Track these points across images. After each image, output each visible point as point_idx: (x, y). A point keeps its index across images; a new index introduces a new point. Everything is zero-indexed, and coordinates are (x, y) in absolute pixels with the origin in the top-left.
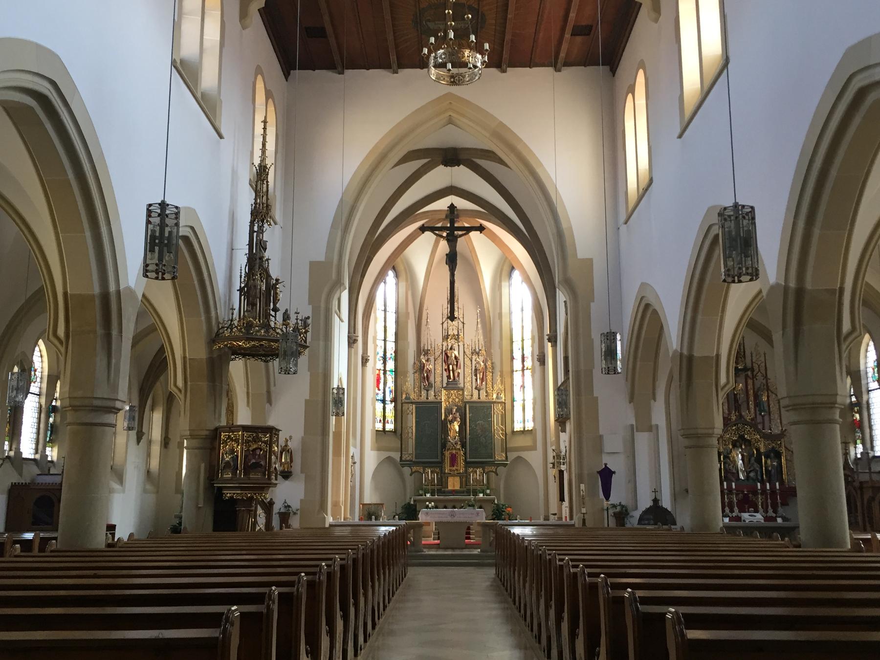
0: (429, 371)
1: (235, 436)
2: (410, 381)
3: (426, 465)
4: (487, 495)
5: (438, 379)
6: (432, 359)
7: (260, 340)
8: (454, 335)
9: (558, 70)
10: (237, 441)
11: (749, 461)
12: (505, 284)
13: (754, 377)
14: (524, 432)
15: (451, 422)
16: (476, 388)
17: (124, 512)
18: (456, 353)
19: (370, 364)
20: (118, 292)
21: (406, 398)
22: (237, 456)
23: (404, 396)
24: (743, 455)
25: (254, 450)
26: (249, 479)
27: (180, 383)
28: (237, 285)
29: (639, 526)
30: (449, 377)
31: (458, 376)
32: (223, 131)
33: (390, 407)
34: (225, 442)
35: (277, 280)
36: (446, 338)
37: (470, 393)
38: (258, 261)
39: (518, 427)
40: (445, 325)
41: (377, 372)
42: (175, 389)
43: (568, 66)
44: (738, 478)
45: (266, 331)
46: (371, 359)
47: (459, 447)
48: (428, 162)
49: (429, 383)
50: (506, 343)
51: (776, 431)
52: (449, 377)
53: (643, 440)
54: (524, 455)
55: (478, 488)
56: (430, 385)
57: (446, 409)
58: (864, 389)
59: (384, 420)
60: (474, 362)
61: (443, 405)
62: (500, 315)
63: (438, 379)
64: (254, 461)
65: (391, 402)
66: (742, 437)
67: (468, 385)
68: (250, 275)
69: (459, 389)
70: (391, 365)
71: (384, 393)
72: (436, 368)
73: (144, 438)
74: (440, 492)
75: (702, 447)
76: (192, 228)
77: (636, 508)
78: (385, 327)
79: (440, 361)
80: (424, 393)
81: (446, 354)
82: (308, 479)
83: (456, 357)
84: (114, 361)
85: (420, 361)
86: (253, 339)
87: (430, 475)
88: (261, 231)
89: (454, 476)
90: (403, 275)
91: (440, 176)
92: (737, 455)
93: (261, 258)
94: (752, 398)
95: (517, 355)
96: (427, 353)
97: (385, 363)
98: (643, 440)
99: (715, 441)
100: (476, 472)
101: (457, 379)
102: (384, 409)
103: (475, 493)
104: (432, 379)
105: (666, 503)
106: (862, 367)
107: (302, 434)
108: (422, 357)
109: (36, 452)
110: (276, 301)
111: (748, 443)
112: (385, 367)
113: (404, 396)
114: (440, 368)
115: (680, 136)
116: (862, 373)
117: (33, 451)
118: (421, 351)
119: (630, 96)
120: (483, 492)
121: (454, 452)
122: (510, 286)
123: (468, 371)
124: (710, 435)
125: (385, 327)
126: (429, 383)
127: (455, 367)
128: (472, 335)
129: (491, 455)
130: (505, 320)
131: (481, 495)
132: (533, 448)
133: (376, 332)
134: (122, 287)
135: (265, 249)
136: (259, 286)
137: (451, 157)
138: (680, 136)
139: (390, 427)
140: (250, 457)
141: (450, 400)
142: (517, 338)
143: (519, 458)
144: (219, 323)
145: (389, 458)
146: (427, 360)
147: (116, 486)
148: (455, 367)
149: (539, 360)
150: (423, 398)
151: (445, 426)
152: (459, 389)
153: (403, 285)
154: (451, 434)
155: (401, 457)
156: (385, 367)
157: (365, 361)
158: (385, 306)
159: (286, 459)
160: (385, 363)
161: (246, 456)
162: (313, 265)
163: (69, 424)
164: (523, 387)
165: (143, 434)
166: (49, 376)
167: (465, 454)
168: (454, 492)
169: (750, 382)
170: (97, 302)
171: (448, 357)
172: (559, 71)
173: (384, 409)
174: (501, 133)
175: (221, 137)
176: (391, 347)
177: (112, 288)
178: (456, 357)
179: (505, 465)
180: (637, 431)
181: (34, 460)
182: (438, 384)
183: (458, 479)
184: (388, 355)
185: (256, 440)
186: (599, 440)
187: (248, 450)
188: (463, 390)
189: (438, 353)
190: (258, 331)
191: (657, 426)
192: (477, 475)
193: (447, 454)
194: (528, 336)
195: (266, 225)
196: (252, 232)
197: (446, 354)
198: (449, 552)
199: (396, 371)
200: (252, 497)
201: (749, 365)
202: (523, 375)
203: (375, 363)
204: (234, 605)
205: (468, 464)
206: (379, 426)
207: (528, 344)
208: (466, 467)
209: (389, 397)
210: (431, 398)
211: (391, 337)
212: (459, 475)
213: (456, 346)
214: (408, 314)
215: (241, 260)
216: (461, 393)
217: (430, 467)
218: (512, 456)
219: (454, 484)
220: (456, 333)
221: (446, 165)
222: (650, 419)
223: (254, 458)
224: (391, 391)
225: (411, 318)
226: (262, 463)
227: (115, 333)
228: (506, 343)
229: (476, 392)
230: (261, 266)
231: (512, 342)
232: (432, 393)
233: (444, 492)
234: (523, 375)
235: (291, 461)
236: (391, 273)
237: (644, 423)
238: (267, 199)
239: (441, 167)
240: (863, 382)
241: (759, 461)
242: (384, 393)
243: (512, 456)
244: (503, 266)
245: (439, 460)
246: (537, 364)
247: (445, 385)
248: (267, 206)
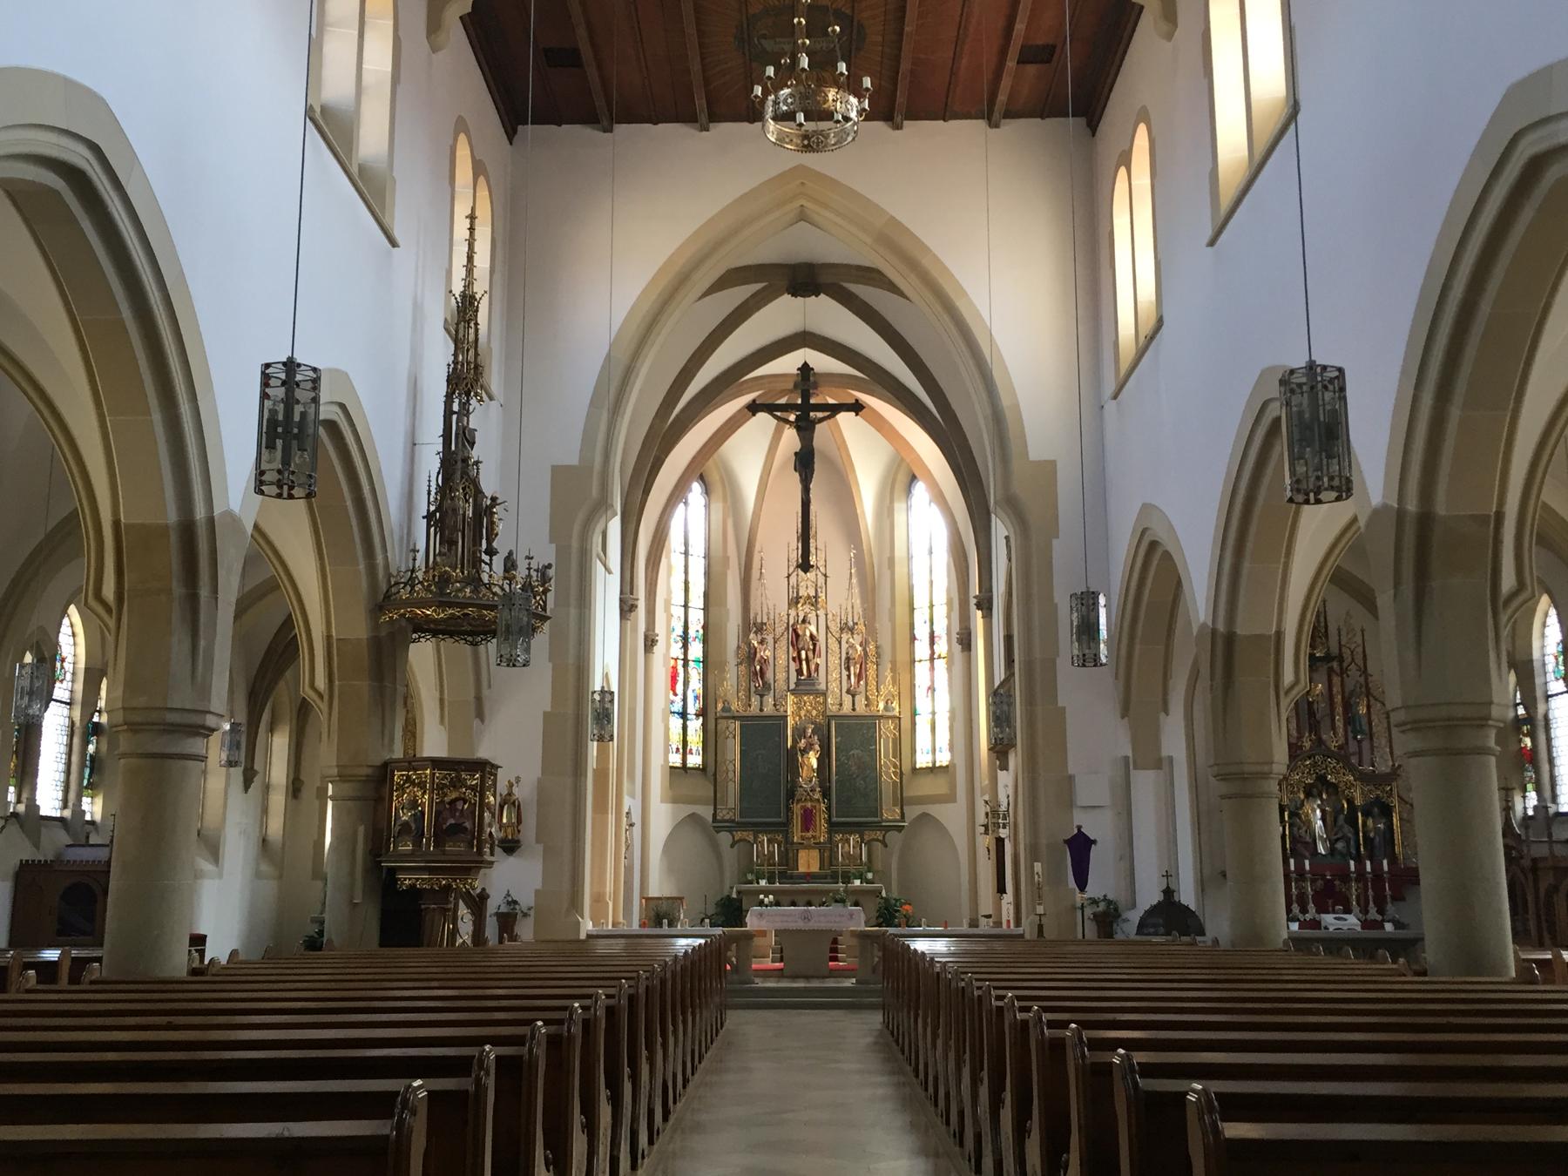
0: (764, 661)
1: (419, 776)
2: (731, 678)
3: (759, 828)
4: (868, 882)
5: (781, 676)
6: (770, 639)
7: (463, 606)
8: (809, 597)
9: (994, 124)
10: (422, 785)
11: (1335, 821)
12: (899, 506)
13: (1343, 672)
14: (933, 770)
15: (804, 751)
16: (848, 692)
17: (221, 912)
18: (813, 628)
19: (659, 649)
21: (723, 709)
22: (423, 813)
23: (720, 706)
24: (1323, 811)
25: (453, 802)
26: (444, 853)
27: (321, 682)
28: (422, 508)
29: (1138, 938)
30: (800, 672)
31: (817, 669)
32: (398, 234)
33: (695, 725)
34: (401, 788)
35: (494, 499)
36: (794, 602)
37: (838, 701)
38: (459, 464)
39: (923, 761)
40: (793, 579)
41: (672, 662)
42: (312, 693)
43: (1013, 117)
44: (1315, 852)
45: (474, 590)
46: (661, 639)
47: (817, 796)
48: (763, 289)
49: (765, 683)
50: (901, 610)
51: (1383, 767)
52: (800, 672)
53: (1145, 784)
54: (934, 810)
55: (852, 869)
56: (767, 687)
57: (795, 729)
58: (1539, 694)
59: (685, 749)
60: (844, 646)
61: (790, 722)
62: (892, 561)
63: (781, 676)
64: (452, 821)
65: (697, 715)
66: (1322, 779)
67: (834, 686)
68: (445, 490)
69: (818, 693)
70: (696, 650)
71: (685, 700)
72: (777, 656)
73: (257, 781)
74: (784, 877)
75: (1251, 796)
76: (342, 406)
77: (1134, 906)
78: (686, 583)
79: (783, 643)
80: (755, 700)
81: (795, 631)
82: (549, 853)
83: (812, 636)
84: (202, 643)
85: (749, 644)
86: (451, 605)
87: (765, 845)
88: (465, 411)
89: (808, 847)
90: (717, 490)
91: (784, 314)
92: (1314, 811)
93: (465, 460)
94: (1339, 709)
95: (922, 632)
96: (760, 628)
97: (685, 646)
98: (1145, 784)
99: (1274, 787)
100: (848, 841)
101: (814, 675)
102: (685, 728)
103: (847, 879)
104: (769, 675)
105: (1187, 896)
106: (1536, 655)
107: (539, 773)
108: (752, 636)
109: (65, 806)
110: (491, 536)
111: (1333, 789)
112: (686, 654)
113: (720, 706)
114: (784, 657)
115: (1212, 243)
116: (1537, 665)
117: (58, 804)
118: (751, 626)
119: (1122, 171)
120: (861, 876)
121: (809, 805)
122: (908, 509)
123: (834, 661)
124: (1265, 776)
125: (686, 583)
126: (765, 683)
127: (810, 654)
128: (841, 597)
129: (876, 812)
130: (900, 570)
131: (857, 882)
132: (950, 798)
133: (669, 592)
135: (472, 444)
136: (461, 510)
137: (804, 279)
138: (1212, 243)
139: (695, 760)
140: (446, 814)
141: (803, 713)
142: (921, 602)
143: (925, 815)
144: (390, 575)
145: (693, 816)
146: (762, 642)
147: (206, 866)
148: (810, 654)
149: (960, 641)
150: (754, 709)
151: (792, 760)
152: (818, 693)
153: (717, 507)
154: (804, 773)
155: (715, 815)
156: (686, 654)
157: (650, 643)
158: (686, 544)
159: (509, 817)
160: (685, 646)
161: (438, 813)
162: (557, 471)
164: (932, 689)
165: (255, 773)
166: (87, 670)
167: (829, 808)
168: (809, 877)
169: (1336, 680)
171: (797, 636)
172: (997, 126)
173: (685, 728)
174: (893, 238)
175: (394, 243)
176: (696, 618)
178: (812, 636)
179: (900, 829)
180: (1135, 768)
181: (61, 820)
182: (781, 684)
183: (815, 854)
184: (692, 633)
185: (457, 783)
186: (1067, 784)
187: (442, 802)
188: (824, 694)
189: (780, 629)
190: (460, 590)
191: (1171, 759)
192: (849, 846)
193: (797, 809)
194: (941, 598)
195: (473, 401)
196: (448, 413)
197: (795, 631)
198: (800, 984)
199: (705, 661)
200: (449, 886)
201: (1335, 650)
202: (932, 668)
203: (668, 646)
204: (416, 1077)
205: (833, 827)
206: (676, 760)
207: (941, 613)
208: (830, 832)
209: (692, 708)
210: (769, 709)
211: (697, 600)
212: (818, 846)
213: (812, 617)
214: (726, 559)
215: (430, 463)
216: (821, 699)
217: (766, 832)
218: (912, 812)
219: (808, 862)
220: (812, 593)
221: (795, 293)
222: (1158, 747)
223: (453, 817)
224: (697, 698)
225: (733, 566)
226: (468, 825)
227: (204, 593)
228: (901, 610)
229: (847, 699)
230: (465, 473)
231: (912, 609)
232: (769, 700)
233: (791, 877)
234: (932, 668)
235: (519, 821)
236: (696, 487)
237: (1147, 754)
238: (477, 355)
239: (786, 298)
240: (1538, 681)
241: (1352, 821)
242: (685, 700)
243: (912, 812)
244: (896, 473)
245: (782, 819)
246: (957, 648)
247: (792, 686)
248: (476, 367)
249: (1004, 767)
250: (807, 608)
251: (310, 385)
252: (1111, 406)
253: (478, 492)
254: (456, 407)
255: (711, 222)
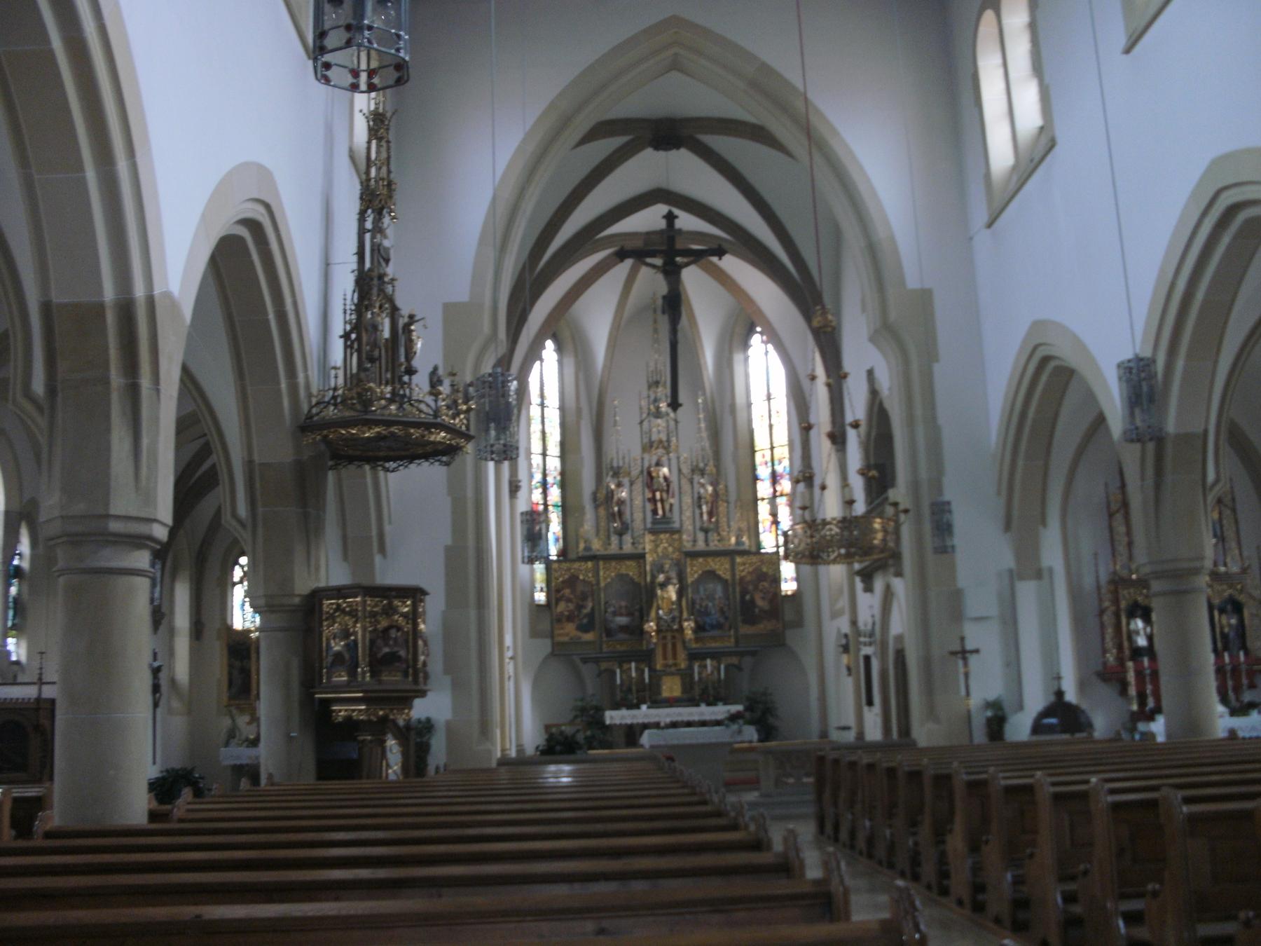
0: (621, 502)
1: (350, 604)
5: (638, 516)
6: (626, 481)
7: (389, 423)
8: (661, 441)
10: (353, 613)
12: (738, 358)
15: (663, 586)
17: (136, 753)
19: (522, 494)
20: (151, 301)
22: (355, 642)
23: (582, 546)
25: (386, 630)
26: (380, 682)
27: (242, 511)
28: (338, 326)
29: (1035, 738)
31: (671, 510)
34: (332, 618)
35: (411, 317)
36: (648, 446)
38: (375, 282)
40: (645, 424)
42: (234, 523)
45: (387, 420)
46: (524, 484)
48: (632, 141)
49: (623, 523)
52: (655, 512)
53: (1027, 592)
57: (653, 564)
60: (696, 486)
61: (649, 558)
63: (638, 516)
64: (386, 650)
67: (688, 525)
68: (363, 304)
69: (673, 532)
70: (555, 494)
73: (165, 622)
75: (1186, 592)
76: (268, 207)
77: (1020, 707)
79: (638, 486)
83: (665, 478)
84: (145, 441)
86: (377, 423)
88: (378, 229)
89: (672, 674)
91: (647, 168)
93: (381, 277)
95: (763, 472)
96: (616, 473)
97: (545, 493)
98: (1027, 592)
99: (1204, 579)
101: (668, 514)
104: (627, 516)
105: (1071, 696)
110: (410, 354)
113: (582, 546)
115: (1128, 51)
119: (989, 15)
122: (746, 359)
123: (687, 500)
124: (1196, 571)
126: (623, 523)
127: (665, 495)
130: (741, 416)
134: (157, 292)
135: (387, 261)
136: (378, 334)
137: (668, 133)
138: (1128, 51)
140: (379, 642)
141: (660, 550)
142: (761, 441)
144: (310, 395)
146: (619, 485)
152: (673, 532)
160: (545, 493)
161: (372, 642)
162: (448, 308)
163: (62, 572)
165: (163, 615)
170: (110, 318)
174: (766, 84)
176: (554, 464)
177: (139, 292)
182: (638, 524)
184: (550, 480)
185: (390, 611)
186: (956, 599)
187: (375, 630)
188: (679, 531)
189: (635, 472)
190: (385, 407)
191: (1051, 570)
194: (782, 436)
195: (386, 221)
196: (362, 232)
197: (649, 473)
200: (384, 720)
203: (530, 492)
207: (782, 452)
212: (679, 672)
213: (664, 459)
215: (344, 284)
216: (676, 536)
220: (664, 438)
221: (657, 148)
223: (387, 645)
224: (557, 540)
225: (588, 417)
226: (402, 653)
227: (145, 382)
229: (701, 536)
230: (381, 291)
232: (627, 539)
236: (549, 344)
237: (1028, 565)
238: (389, 172)
239: (649, 152)
247: (649, 526)
248: (390, 184)
249: (869, 589)
250: (661, 451)
251: (330, 42)
252: (982, 239)
253: (394, 311)
254: (369, 225)
255: (552, 106)
